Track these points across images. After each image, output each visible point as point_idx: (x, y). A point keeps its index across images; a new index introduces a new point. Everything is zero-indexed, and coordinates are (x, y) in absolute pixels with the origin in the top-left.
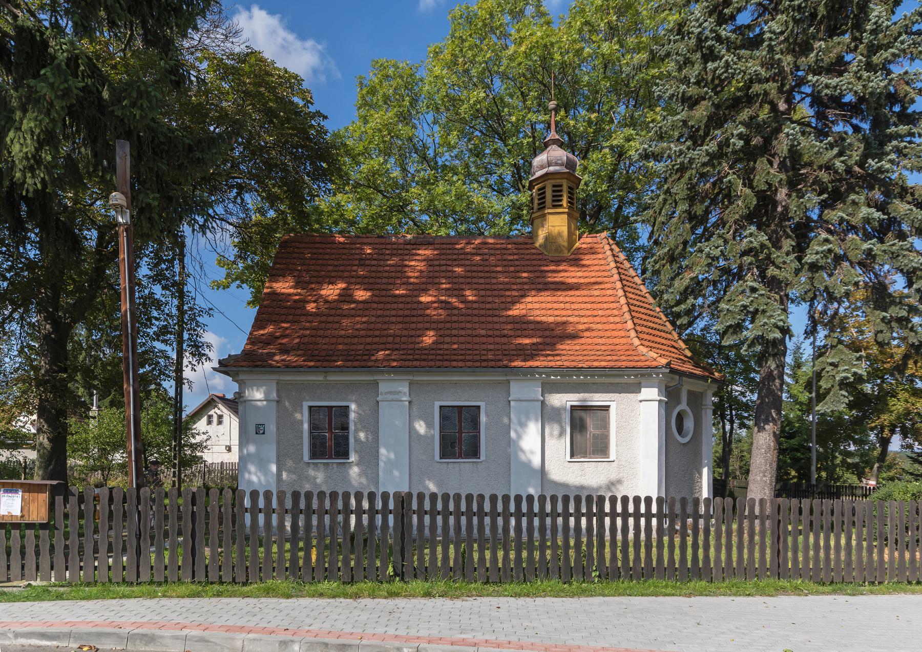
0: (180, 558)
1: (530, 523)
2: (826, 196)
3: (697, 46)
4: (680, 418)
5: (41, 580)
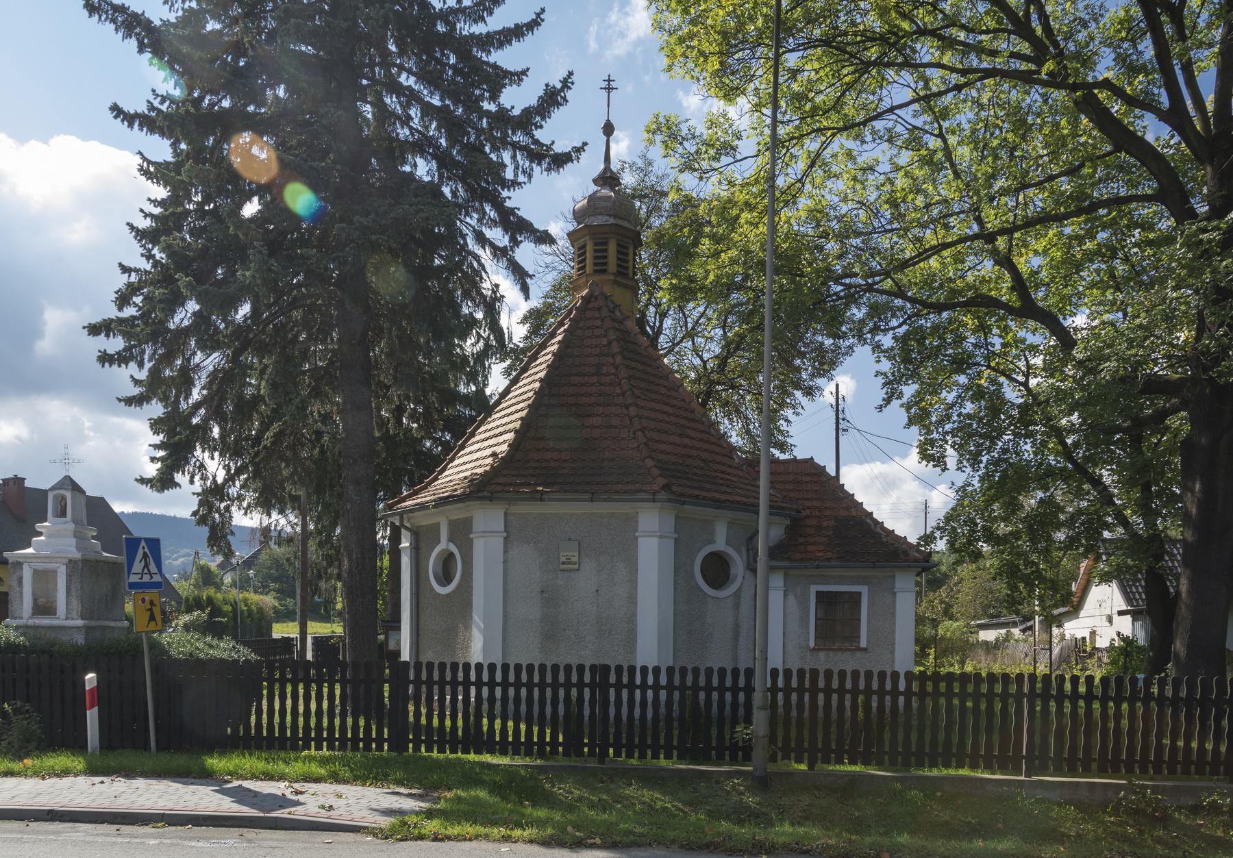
3: (655, 191)
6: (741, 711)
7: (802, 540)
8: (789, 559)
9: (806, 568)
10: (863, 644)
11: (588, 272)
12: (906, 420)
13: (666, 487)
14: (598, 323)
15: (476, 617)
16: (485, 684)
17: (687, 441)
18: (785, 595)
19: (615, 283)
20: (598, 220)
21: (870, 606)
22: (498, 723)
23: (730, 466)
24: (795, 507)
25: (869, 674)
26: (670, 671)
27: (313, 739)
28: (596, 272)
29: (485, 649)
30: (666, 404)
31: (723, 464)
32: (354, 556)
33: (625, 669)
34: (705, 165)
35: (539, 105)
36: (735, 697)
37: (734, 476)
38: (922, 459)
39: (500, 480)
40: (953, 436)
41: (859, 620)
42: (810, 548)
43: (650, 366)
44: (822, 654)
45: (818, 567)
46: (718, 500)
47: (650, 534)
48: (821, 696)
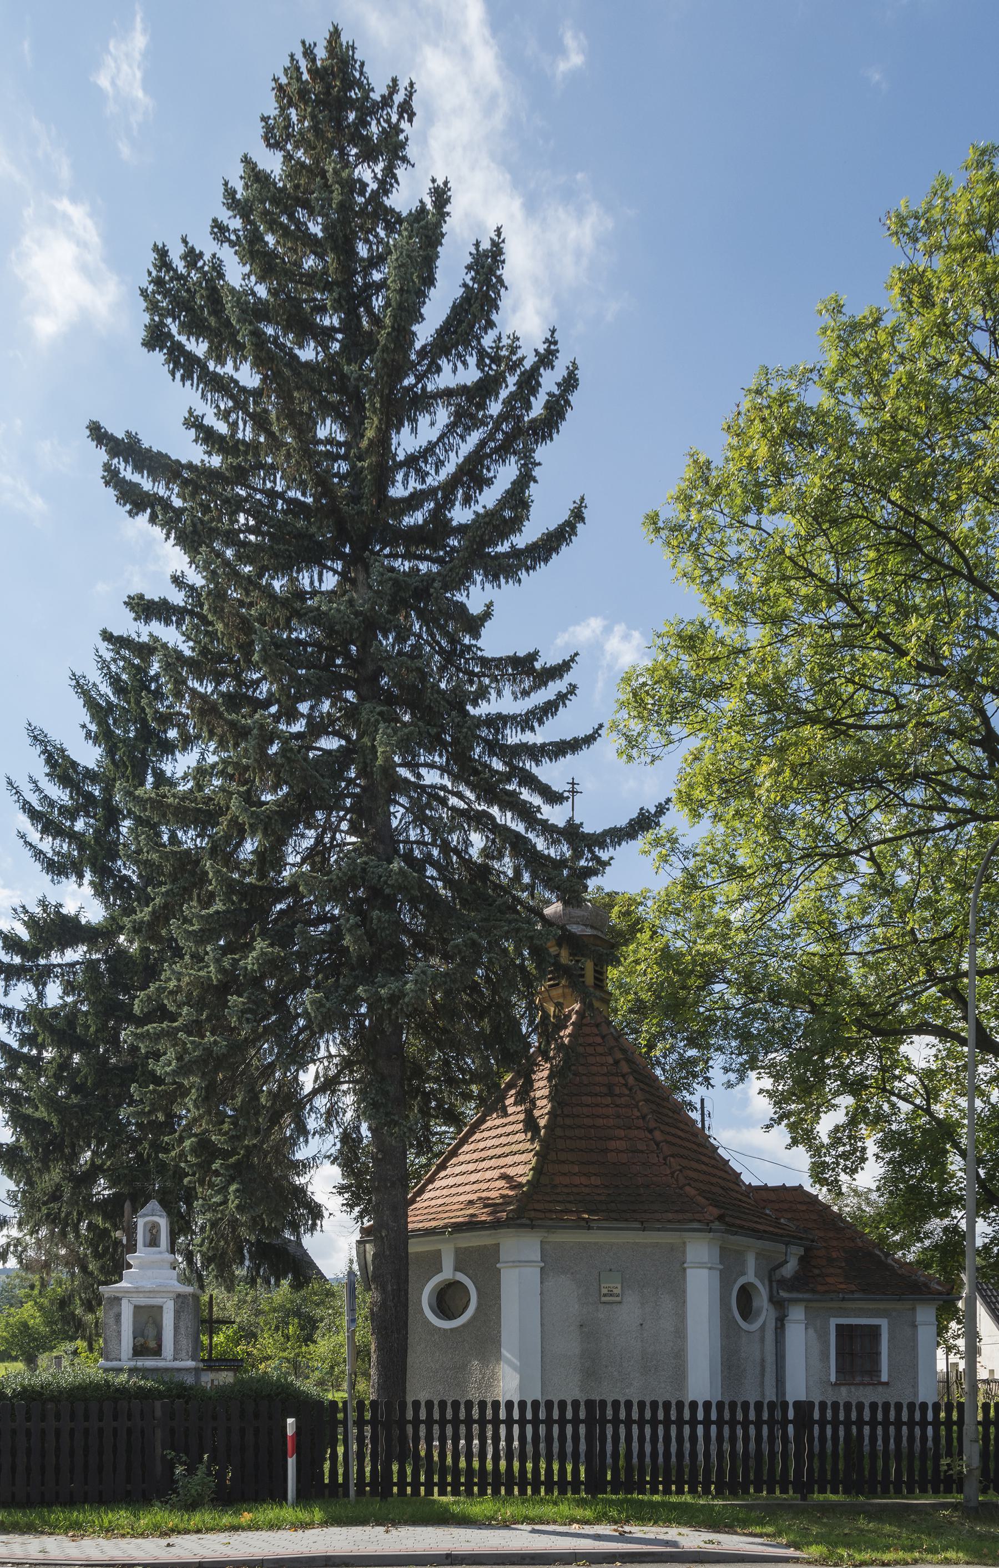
0: (609, 1473)
2: (285, 789)
4: (746, 1294)
5: (846, 1492)
7: (817, 1271)
8: (813, 1291)
9: (832, 1300)
10: (884, 1378)
14: (599, 1040)
15: (504, 1352)
16: (569, 1421)
25: (629, 1404)
26: (720, 1405)
29: (522, 1387)
32: (389, 1288)
33: (436, 1403)
36: (949, 1432)
39: (537, 1206)
41: (878, 1354)
42: (830, 1280)
44: (844, 1390)
45: (843, 1299)
46: (757, 1231)
47: (700, 1266)
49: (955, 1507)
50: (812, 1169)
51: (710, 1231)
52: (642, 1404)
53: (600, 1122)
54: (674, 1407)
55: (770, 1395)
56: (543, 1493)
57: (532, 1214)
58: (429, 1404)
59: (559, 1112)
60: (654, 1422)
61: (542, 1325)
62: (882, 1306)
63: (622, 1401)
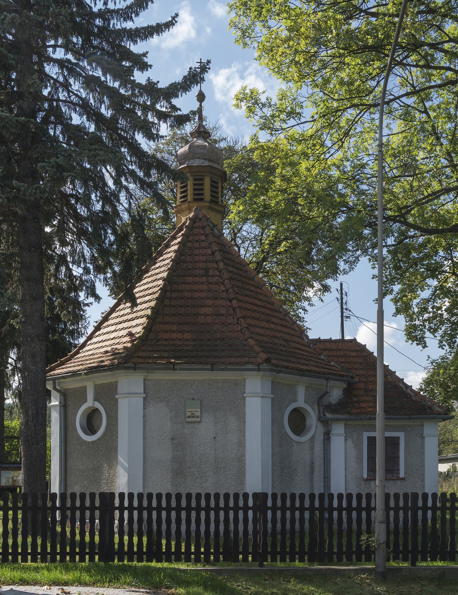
1: (293, 515)
6: (364, 527)
7: (355, 399)
8: (349, 413)
9: (362, 419)
10: (402, 475)
11: (189, 200)
12: (394, 311)
13: (267, 361)
14: (203, 238)
15: (120, 459)
16: (173, 509)
17: (272, 326)
18: (346, 440)
19: (210, 208)
20: (196, 163)
21: (407, 446)
22: (135, 539)
23: (302, 345)
24: (351, 375)
25: (189, 496)
27: (20, 554)
28: (195, 200)
30: (256, 298)
31: (298, 343)
32: (30, 413)
33: (288, 495)
34: (277, 125)
35: (183, 82)
37: (306, 352)
38: (408, 339)
39: (141, 354)
40: (429, 323)
41: (398, 457)
42: (363, 405)
43: (241, 270)
46: (301, 370)
47: (255, 395)
48: (420, 513)
49: (369, 571)
50: (406, 330)
51: (259, 370)
52: (217, 496)
53: (196, 295)
54: (164, 497)
55: (318, 489)
56: (20, 561)
57: (136, 360)
58: (83, 496)
59: (169, 288)
60: (208, 509)
61: (144, 438)
62: (400, 423)
63: (364, 494)
